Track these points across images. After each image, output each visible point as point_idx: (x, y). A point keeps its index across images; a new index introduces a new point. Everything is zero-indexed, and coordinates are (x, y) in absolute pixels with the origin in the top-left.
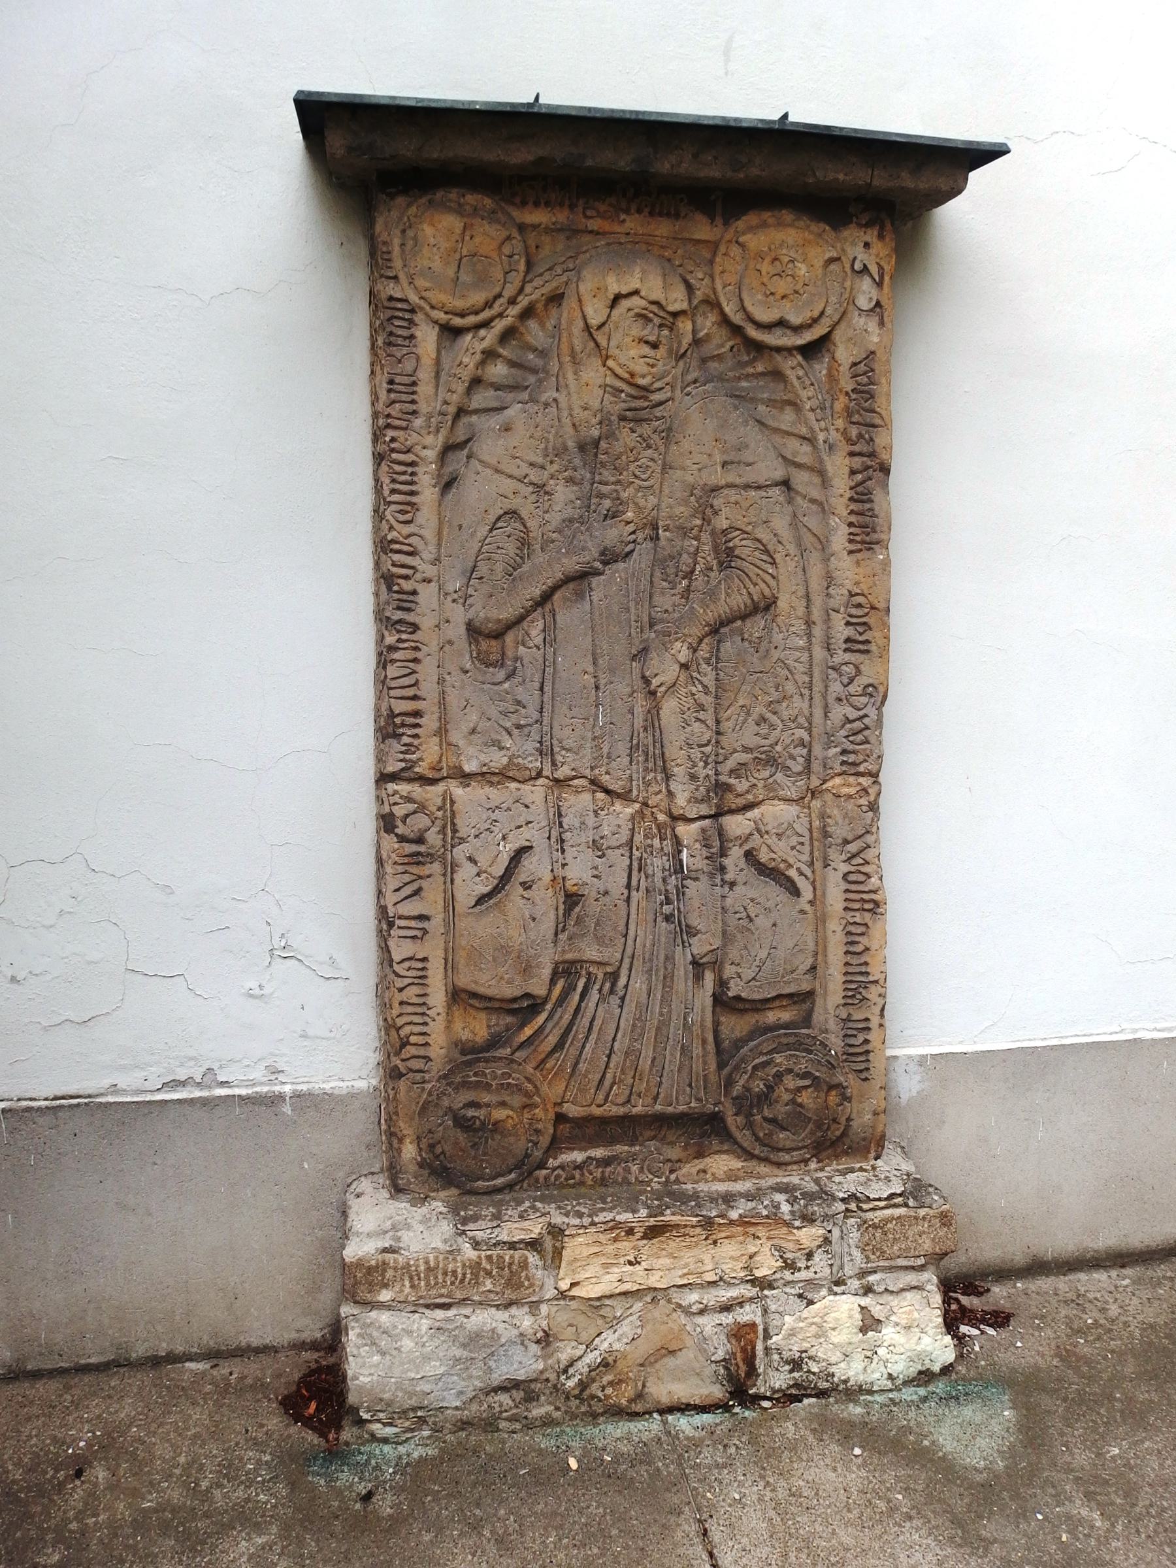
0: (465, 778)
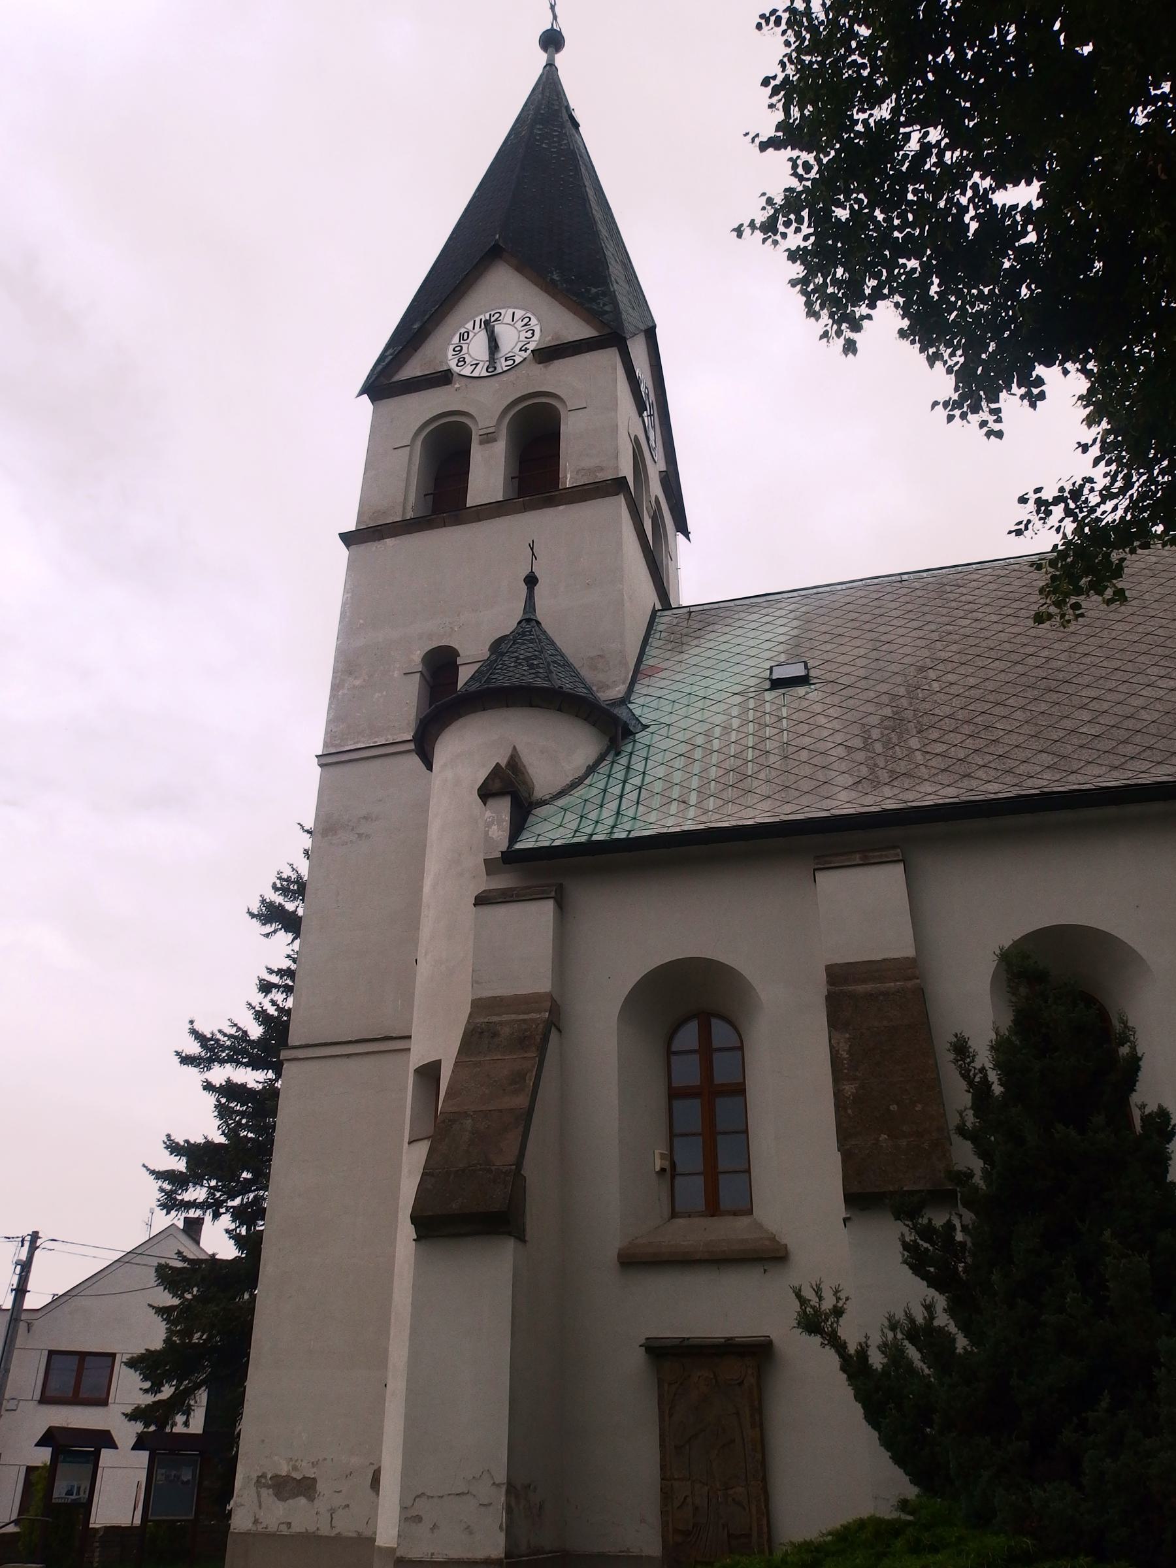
0: (675, 1479)
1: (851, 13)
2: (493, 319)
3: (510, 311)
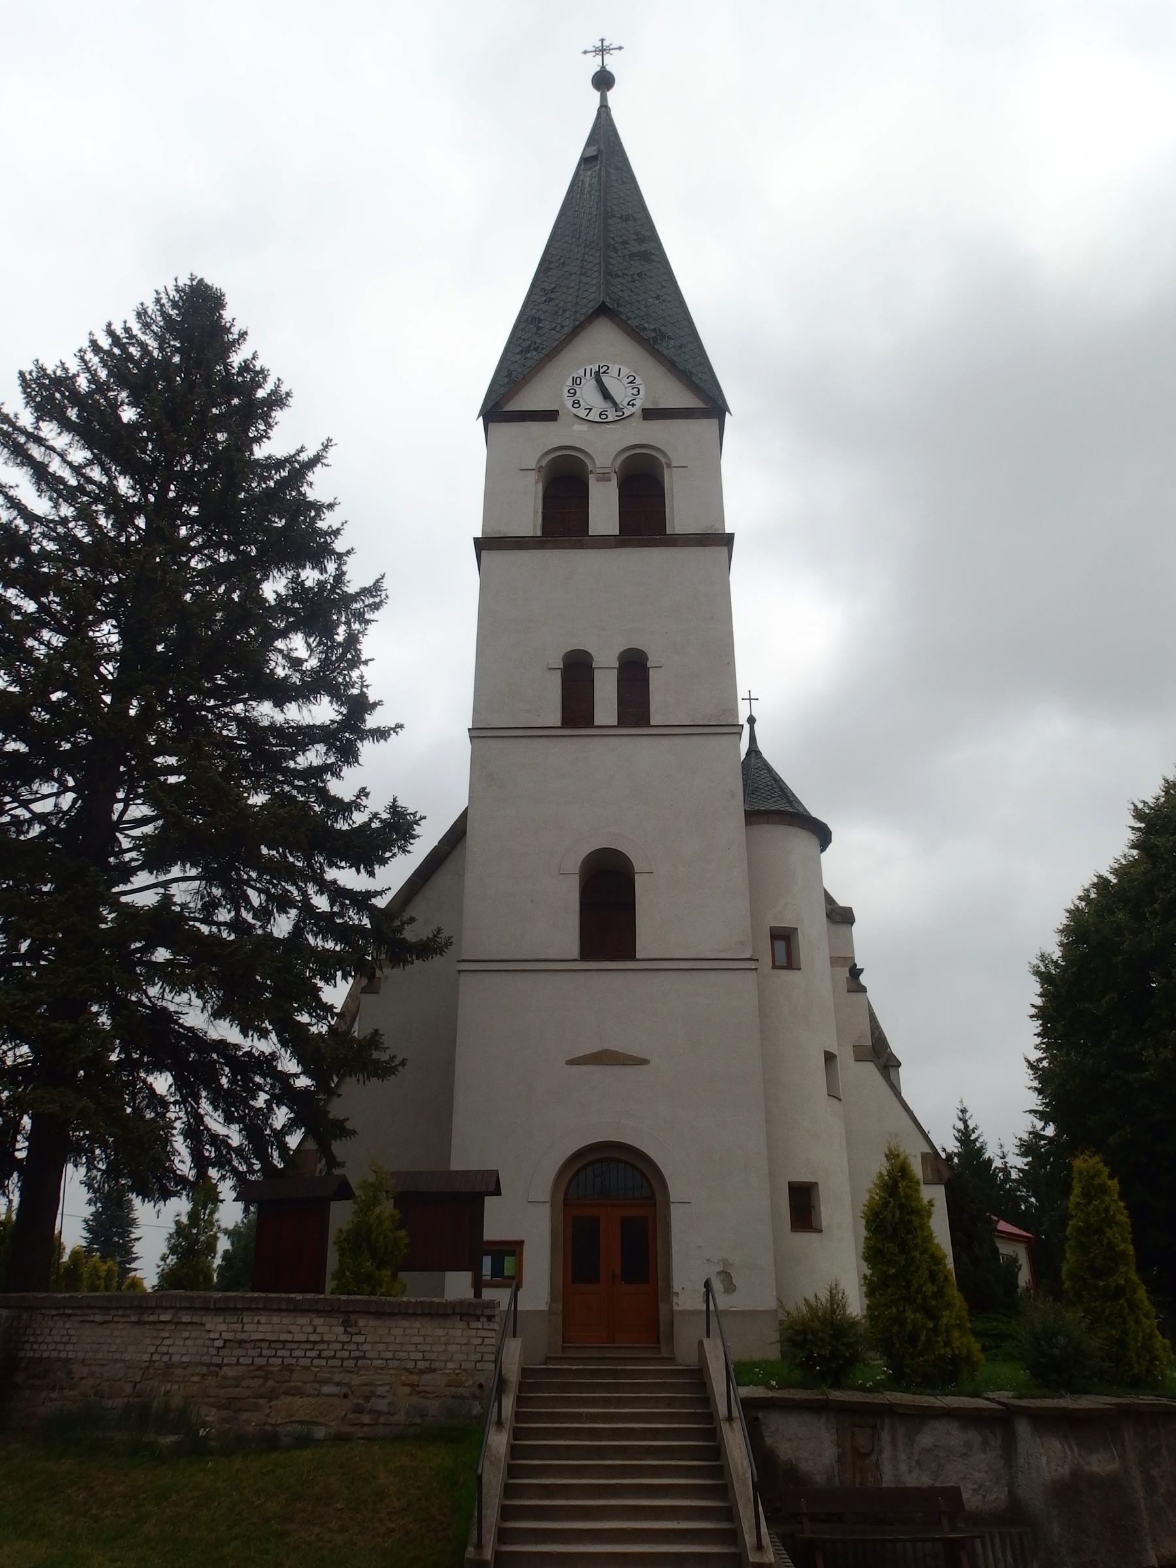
1: (152, 740)
2: (602, 371)
3: (617, 367)
